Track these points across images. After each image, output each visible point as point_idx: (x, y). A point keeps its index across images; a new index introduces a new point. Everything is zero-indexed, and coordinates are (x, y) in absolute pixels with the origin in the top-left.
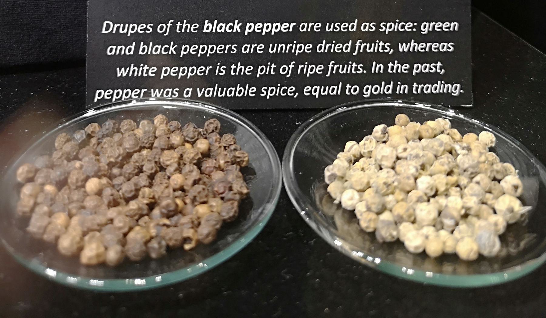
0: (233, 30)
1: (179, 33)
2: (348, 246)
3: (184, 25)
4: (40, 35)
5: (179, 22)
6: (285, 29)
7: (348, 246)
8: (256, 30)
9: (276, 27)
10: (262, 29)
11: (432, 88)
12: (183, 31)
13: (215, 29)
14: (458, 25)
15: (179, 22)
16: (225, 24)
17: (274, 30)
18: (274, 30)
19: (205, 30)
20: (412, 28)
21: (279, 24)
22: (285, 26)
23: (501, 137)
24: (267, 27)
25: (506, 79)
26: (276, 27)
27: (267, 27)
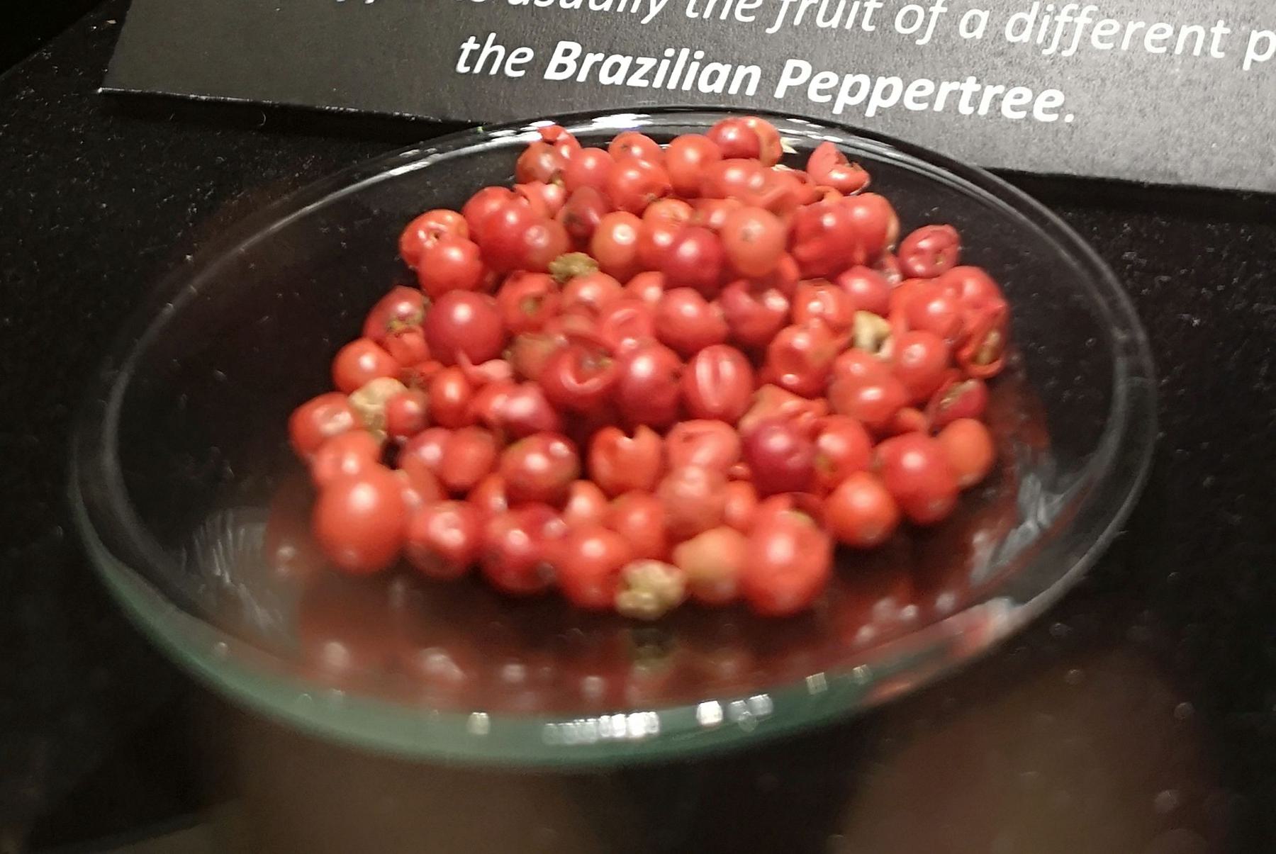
0: (472, 69)
1: (465, 74)
2: (670, 185)
3: (487, 50)
4: (1204, 127)
5: (472, 39)
6: (917, 100)
7: (670, 185)
8: (909, 104)
9: (886, 93)
10: (834, 93)
11: (829, 185)
12: (477, 69)
13: (677, 82)
14: (591, 131)
15: (472, 39)
16: (728, 67)
17: (876, 101)
18: (876, 101)
19: (551, 74)
20: (1059, 110)
21: (896, 82)
22: (921, 88)
23: (290, 213)
24: (854, 91)
25: (342, 230)
26: (886, 93)
27: (854, 91)
